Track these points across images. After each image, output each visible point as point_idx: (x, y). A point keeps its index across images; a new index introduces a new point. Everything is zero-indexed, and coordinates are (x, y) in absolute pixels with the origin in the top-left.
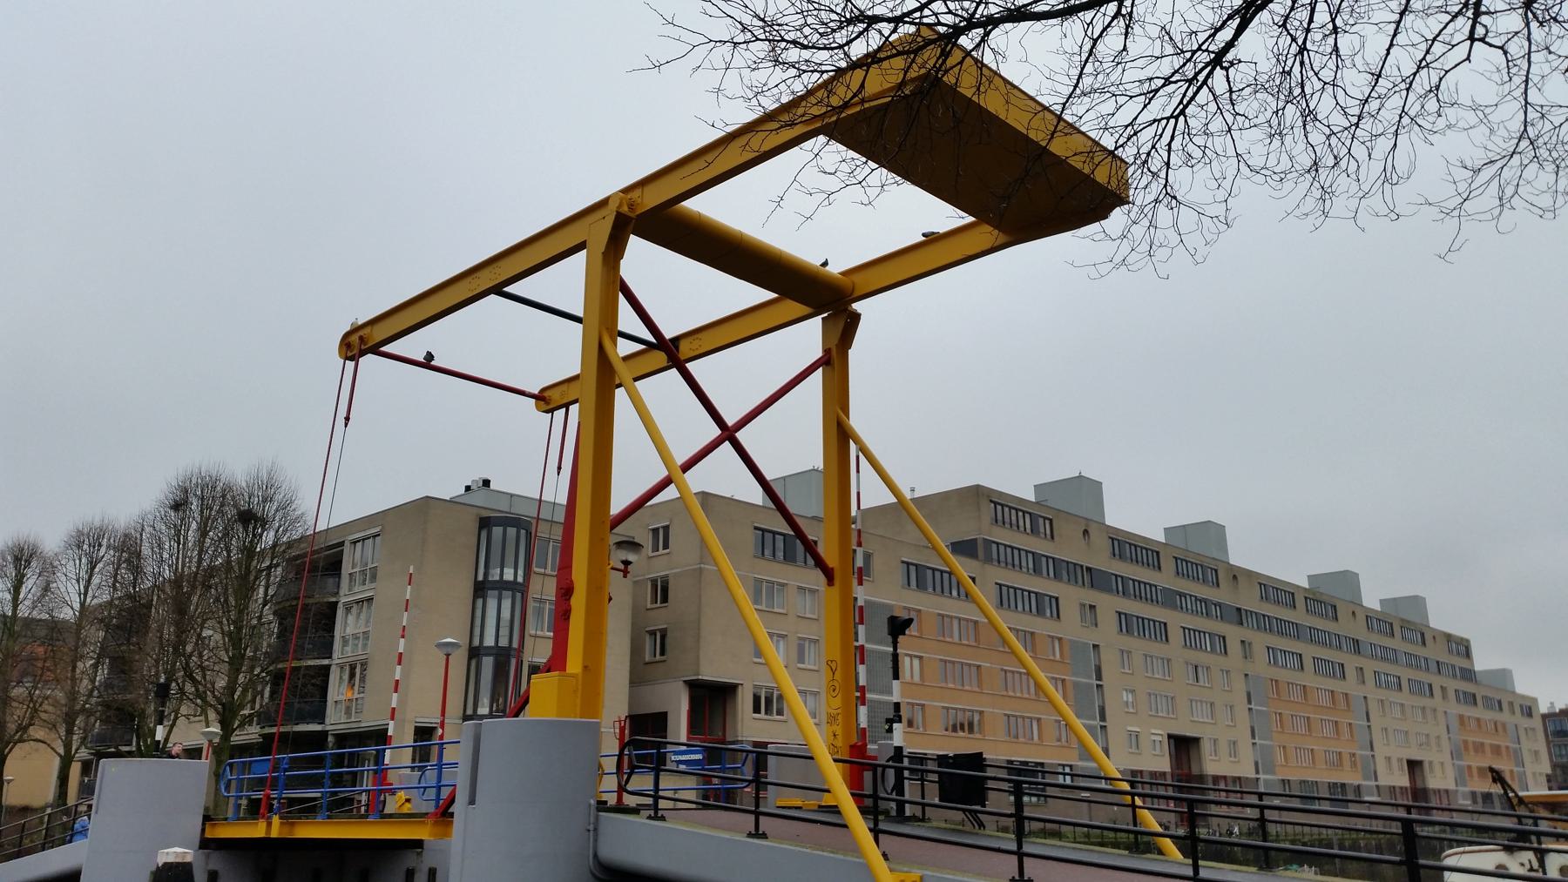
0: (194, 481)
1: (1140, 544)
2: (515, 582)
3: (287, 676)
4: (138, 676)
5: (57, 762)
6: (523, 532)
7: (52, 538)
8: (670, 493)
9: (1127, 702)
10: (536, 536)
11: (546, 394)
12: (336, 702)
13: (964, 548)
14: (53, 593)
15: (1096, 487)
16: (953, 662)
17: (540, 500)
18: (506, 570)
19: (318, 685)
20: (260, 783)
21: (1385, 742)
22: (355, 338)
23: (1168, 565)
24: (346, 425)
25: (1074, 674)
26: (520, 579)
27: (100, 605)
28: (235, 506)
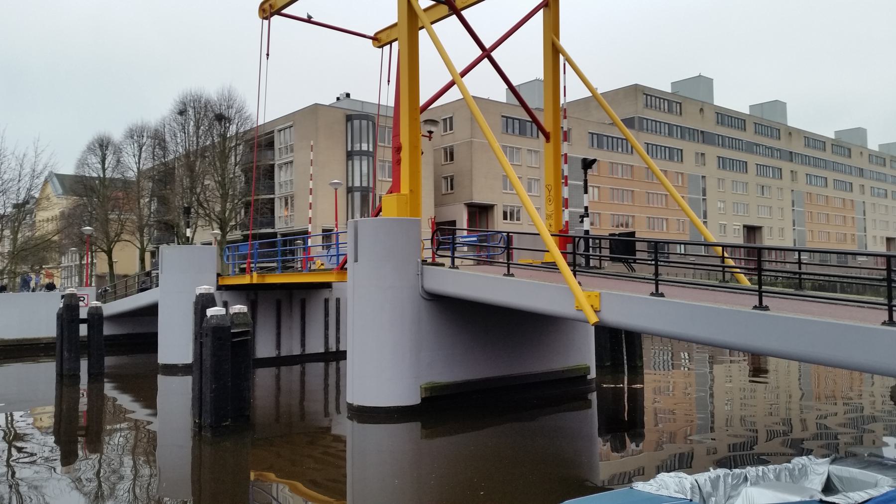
0: (189, 98)
1: (734, 116)
2: (368, 151)
3: (252, 204)
4: (173, 205)
5: (138, 252)
6: (371, 123)
7: (117, 134)
8: (454, 94)
9: (720, 208)
10: (378, 125)
11: (378, 36)
12: (280, 217)
13: (629, 122)
14: (122, 164)
15: (710, 81)
16: (618, 189)
17: (379, 105)
18: (363, 145)
19: (269, 208)
20: (244, 257)
21: (874, 227)
22: (267, 6)
23: (750, 127)
24: (268, 58)
25: (689, 193)
26: (371, 150)
27: (148, 169)
28: (213, 111)
